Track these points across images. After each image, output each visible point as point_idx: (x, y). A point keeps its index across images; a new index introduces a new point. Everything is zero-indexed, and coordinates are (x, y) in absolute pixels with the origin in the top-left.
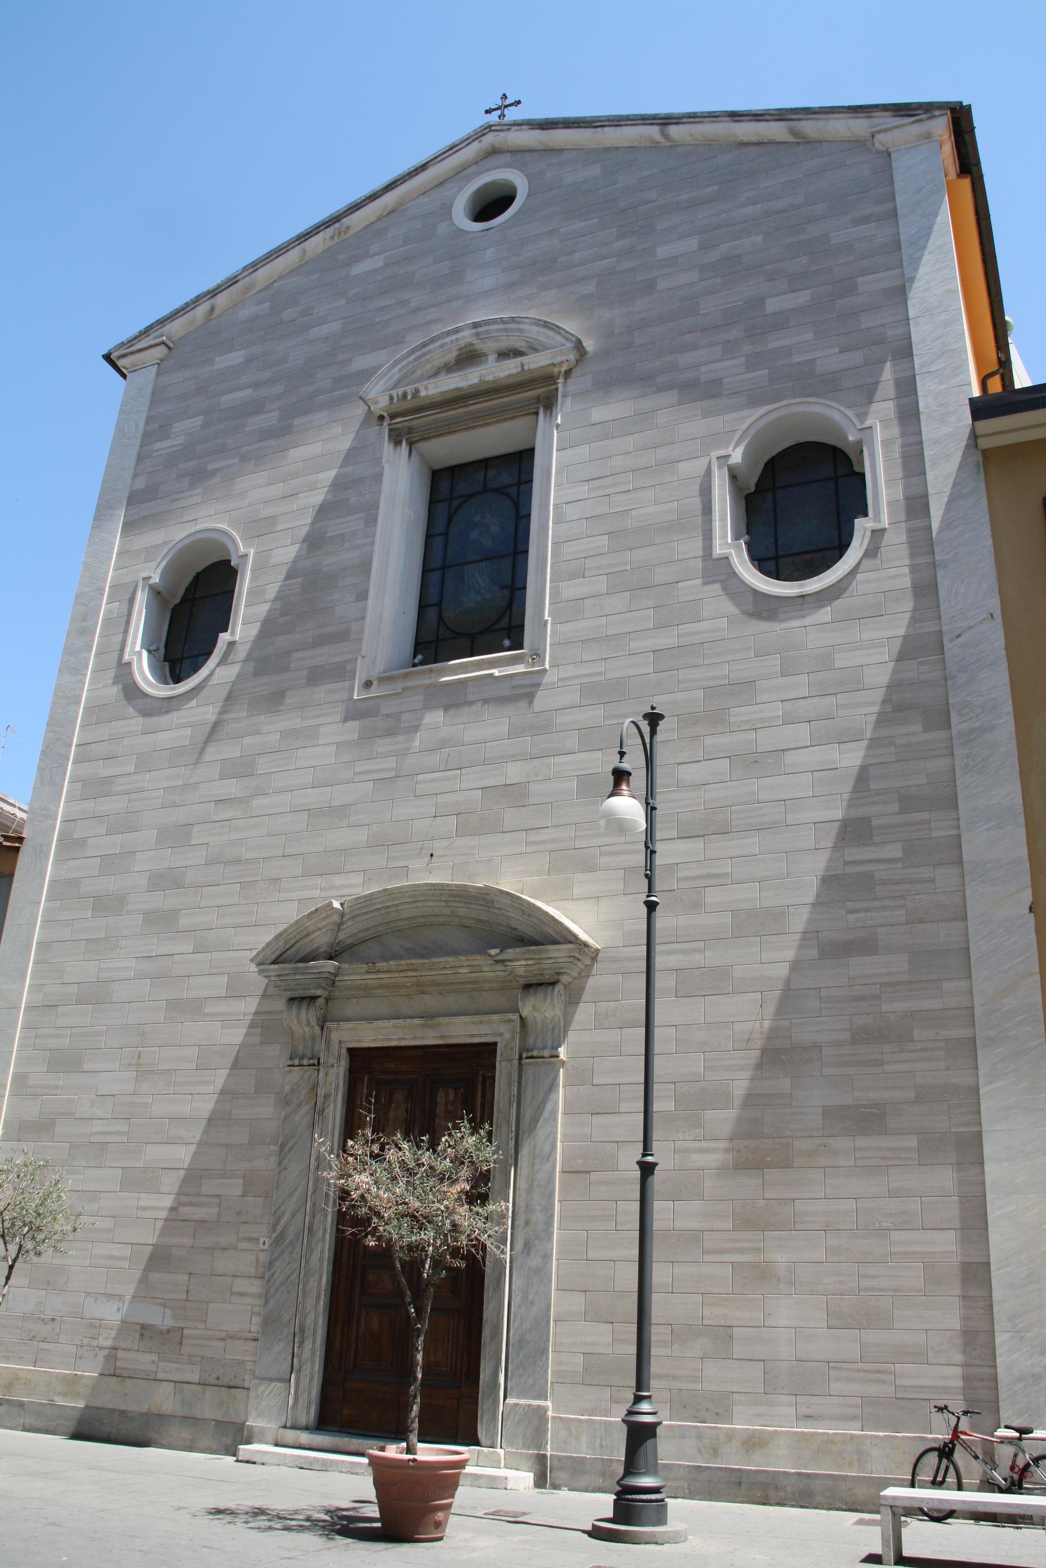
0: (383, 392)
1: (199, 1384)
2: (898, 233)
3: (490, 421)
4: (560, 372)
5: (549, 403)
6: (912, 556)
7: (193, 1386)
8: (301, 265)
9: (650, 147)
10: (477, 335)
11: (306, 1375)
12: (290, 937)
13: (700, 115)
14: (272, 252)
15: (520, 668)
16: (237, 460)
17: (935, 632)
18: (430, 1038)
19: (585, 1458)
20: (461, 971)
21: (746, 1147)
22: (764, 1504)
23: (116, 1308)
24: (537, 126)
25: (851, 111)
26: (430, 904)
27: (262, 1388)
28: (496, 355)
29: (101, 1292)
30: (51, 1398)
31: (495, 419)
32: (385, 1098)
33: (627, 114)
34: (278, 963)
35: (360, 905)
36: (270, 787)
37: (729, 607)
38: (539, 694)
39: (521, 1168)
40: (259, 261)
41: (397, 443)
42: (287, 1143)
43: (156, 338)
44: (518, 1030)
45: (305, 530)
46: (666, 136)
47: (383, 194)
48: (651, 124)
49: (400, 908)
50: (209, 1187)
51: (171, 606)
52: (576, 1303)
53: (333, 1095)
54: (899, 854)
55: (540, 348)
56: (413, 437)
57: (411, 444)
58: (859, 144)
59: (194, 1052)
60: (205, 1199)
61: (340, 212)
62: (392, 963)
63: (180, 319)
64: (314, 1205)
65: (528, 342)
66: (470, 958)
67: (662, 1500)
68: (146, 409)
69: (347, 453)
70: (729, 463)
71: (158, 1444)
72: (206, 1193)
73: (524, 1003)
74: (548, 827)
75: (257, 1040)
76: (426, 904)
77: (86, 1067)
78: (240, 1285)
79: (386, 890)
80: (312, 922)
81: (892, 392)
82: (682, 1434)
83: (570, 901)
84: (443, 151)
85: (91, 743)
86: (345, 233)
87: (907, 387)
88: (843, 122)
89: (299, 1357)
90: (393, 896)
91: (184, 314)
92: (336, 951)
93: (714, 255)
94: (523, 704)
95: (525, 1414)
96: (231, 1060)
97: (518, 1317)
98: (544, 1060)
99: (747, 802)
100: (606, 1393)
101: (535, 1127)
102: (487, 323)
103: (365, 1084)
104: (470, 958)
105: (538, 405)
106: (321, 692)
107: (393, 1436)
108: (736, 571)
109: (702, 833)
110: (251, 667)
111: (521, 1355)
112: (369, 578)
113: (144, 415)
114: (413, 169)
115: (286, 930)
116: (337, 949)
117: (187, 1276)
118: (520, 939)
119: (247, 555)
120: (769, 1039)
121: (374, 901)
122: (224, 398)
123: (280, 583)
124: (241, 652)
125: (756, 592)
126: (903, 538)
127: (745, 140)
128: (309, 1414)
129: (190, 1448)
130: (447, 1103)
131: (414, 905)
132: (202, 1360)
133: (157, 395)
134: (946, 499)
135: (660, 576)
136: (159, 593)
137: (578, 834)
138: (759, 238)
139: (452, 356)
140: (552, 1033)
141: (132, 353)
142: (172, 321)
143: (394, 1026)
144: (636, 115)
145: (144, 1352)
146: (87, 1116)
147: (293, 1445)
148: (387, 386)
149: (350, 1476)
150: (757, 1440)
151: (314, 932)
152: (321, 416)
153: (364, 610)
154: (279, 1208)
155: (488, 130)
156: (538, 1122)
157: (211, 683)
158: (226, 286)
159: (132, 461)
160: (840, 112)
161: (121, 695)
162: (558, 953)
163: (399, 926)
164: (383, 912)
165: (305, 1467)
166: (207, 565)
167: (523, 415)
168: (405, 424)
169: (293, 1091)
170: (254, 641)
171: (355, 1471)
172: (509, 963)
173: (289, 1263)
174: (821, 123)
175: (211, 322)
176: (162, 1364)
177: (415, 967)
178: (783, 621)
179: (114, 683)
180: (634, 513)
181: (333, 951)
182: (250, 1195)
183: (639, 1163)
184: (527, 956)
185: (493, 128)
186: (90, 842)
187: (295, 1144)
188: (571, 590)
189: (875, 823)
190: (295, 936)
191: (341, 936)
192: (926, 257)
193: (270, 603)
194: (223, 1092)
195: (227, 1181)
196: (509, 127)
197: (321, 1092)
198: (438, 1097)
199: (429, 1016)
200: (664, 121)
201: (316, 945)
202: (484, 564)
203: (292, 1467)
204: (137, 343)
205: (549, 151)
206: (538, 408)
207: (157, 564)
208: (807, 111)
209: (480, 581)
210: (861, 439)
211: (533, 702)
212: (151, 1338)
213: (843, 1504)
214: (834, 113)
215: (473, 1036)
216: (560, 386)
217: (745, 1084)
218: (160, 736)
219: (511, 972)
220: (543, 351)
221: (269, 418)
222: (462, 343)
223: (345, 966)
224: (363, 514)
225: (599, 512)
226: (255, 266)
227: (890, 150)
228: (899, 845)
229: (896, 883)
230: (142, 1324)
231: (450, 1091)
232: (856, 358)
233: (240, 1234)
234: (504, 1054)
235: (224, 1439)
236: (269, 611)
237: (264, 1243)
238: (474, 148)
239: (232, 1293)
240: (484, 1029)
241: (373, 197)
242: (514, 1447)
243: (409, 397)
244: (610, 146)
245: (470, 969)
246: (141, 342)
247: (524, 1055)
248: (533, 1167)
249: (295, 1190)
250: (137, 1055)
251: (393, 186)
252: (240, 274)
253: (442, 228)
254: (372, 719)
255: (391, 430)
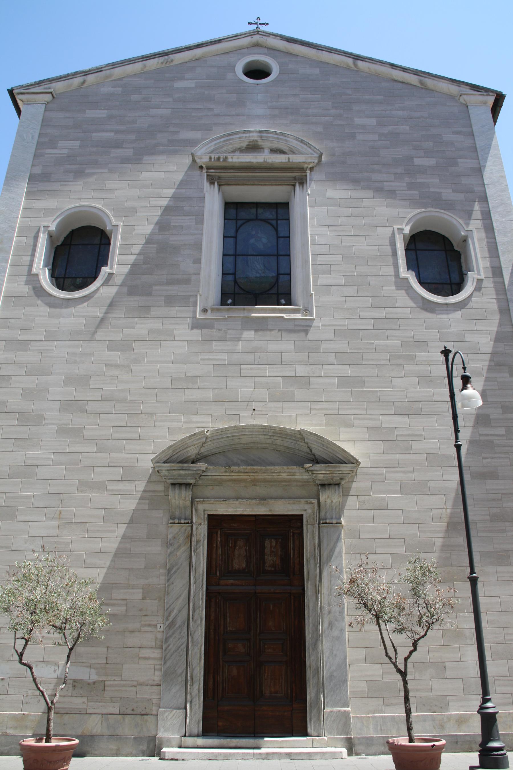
0: (204, 154)
1: (119, 714)
2: (475, 143)
3: (267, 183)
4: (307, 167)
5: (302, 182)
6: (497, 294)
7: (115, 716)
8: (141, 73)
9: (346, 68)
10: (261, 137)
11: (196, 704)
12: (176, 448)
13: (375, 60)
14: (126, 61)
15: (299, 316)
16: (107, 171)
17: (511, 331)
18: (262, 510)
19: (374, 737)
20: (282, 474)
21: (444, 571)
22: (470, 752)
23: (53, 670)
24: (285, 39)
25: (451, 81)
26: (260, 436)
27: (167, 714)
28: (269, 150)
29: (40, 660)
30: (4, 731)
31: (271, 183)
32: (231, 543)
33: (336, 48)
34: (166, 463)
35: (218, 434)
36: (144, 360)
37: (411, 304)
38: (311, 331)
39: (323, 583)
40: (117, 63)
41: (212, 183)
42: (173, 568)
43: (45, 89)
44: (317, 509)
45: (157, 218)
46: (355, 65)
47: (195, 49)
48: (349, 57)
49: (241, 437)
50: (117, 594)
51: (55, 246)
52: (360, 654)
53: (202, 541)
54: (504, 433)
55: (296, 152)
56: (222, 182)
57: (219, 185)
58: (451, 97)
59: (101, 512)
60: (115, 602)
61: (169, 51)
62: (242, 467)
63: (62, 82)
64: (194, 604)
65: (289, 147)
66: (289, 468)
67: (505, 754)
68: (39, 127)
69: (181, 182)
70: (403, 233)
71: (92, 754)
72: (116, 598)
73: (322, 494)
74: (323, 402)
75: (146, 507)
76: (257, 436)
77: (19, 518)
78: (144, 653)
79: (235, 426)
80: (190, 441)
81: (480, 216)
82: (424, 719)
83: (339, 441)
84: (231, 36)
85: (10, 318)
86: (170, 63)
87: (487, 216)
88: (446, 84)
89: (191, 694)
90: (239, 430)
91: (65, 80)
92: (197, 458)
93: (385, 130)
94: (303, 334)
95: (337, 716)
96: (129, 518)
97: (328, 664)
98: (333, 525)
99: (429, 400)
100: (381, 701)
101: (330, 560)
102: (267, 132)
103: (219, 535)
104: (289, 468)
105: (296, 181)
106: (175, 310)
107: (253, 735)
108: (413, 286)
109: (407, 413)
110: (125, 289)
111: (332, 684)
112: (201, 252)
113: (38, 132)
114: (213, 40)
115: (174, 444)
116: (198, 457)
117: (106, 649)
118: (311, 459)
119: (118, 225)
120: (450, 518)
121: (227, 432)
122: (94, 134)
123: (142, 245)
124: (119, 280)
125: (423, 298)
126: (491, 285)
127: (396, 79)
128: (198, 728)
129: (117, 755)
130: (271, 547)
131: (251, 436)
132: (120, 699)
133: (45, 122)
134: (510, 271)
135: (373, 281)
136: (51, 237)
137: (340, 407)
138: (408, 128)
139: (244, 145)
140: (335, 510)
141: (28, 93)
142: (57, 82)
143: (240, 503)
144: (341, 50)
145: (76, 697)
146: (22, 549)
147: (192, 746)
148: (206, 151)
149: (244, 761)
150: (463, 719)
151: (190, 446)
152: (162, 158)
153: (200, 269)
154: (170, 606)
155: (257, 33)
156: (331, 558)
157: (97, 295)
158: (95, 71)
159: (31, 157)
160: (445, 80)
161: (32, 292)
162: (345, 468)
163: (238, 447)
164: (230, 438)
165: (212, 759)
166: (95, 226)
167: (286, 185)
168: (217, 174)
169: (174, 538)
170: (127, 275)
171: (246, 758)
172: (315, 472)
173: (179, 639)
174: (435, 82)
175: (81, 89)
176: (90, 704)
177: (256, 471)
178: (438, 314)
179: (26, 284)
180: (355, 247)
181: (196, 458)
182: (148, 599)
183: (468, 578)
184: (328, 469)
185: (260, 33)
186: (13, 378)
187: (178, 569)
188: (324, 280)
189: (492, 417)
190: (179, 448)
191: (203, 450)
192: (489, 158)
193: (136, 256)
194: (124, 537)
195: (131, 591)
196: (269, 35)
197: (194, 539)
198: (266, 544)
199: (263, 499)
200: (356, 57)
201: (189, 454)
202: (259, 257)
203: (203, 760)
204: (32, 88)
205: (289, 54)
206: (296, 183)
207: (54, 219)
208: (429, 74)
209: (258, 266)
210: (468, 235)
211: (308, 334)
212: (81, 688)
213: (509, 748)
214: (442, 79)
215: (289, 510)
216: (308, 174)
217: (441, 540)
218: (62, 321)
219: (315, 477)
220: (299, 154)
221: (129, 153)
222: (252, 139)
223: (212, 467)
224: (194, 217)
225: (336, 243)
226: (114, 65)
227: (468, 104)
228: (503, 429)
229: (504, 446)
230: (73, 679)
231: (273, 540)
232: (460, 196)
233: (143, 623)
234: (309, 521)
235: (141, 747)
236: (136, 260)
237: (160, 627)
238: (247, 41)
239: (139, 658)
240: (295, 507)
241: (189, 48)
242: (332, 735)
243: (221, 160)
244: (324, 61)
245: (289, 474)
246: (34, 89)
247: (321, 522)
248: (330, 582)
249: (180, 596)
250: (58, 512)
251: (201, 46)
252: (104, 67)
253: (230, 76)
254: (209, 330)
255: (207, 175)
